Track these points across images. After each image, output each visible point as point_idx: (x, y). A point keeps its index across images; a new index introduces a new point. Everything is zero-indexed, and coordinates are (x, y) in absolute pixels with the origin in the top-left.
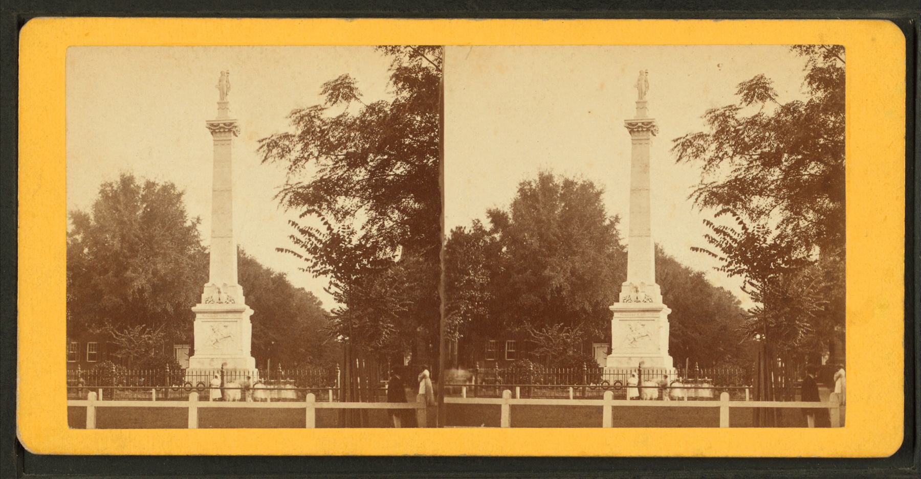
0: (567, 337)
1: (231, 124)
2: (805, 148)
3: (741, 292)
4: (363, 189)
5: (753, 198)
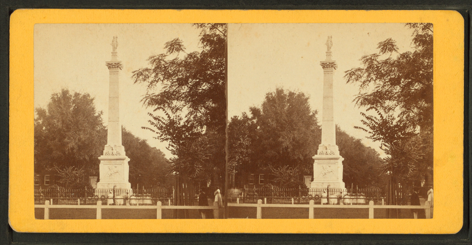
0: (77, 173)
1: (119, 63)
2: (413, 76)
3: (380, 149)
4: (186, 97)
5: (386, 101)
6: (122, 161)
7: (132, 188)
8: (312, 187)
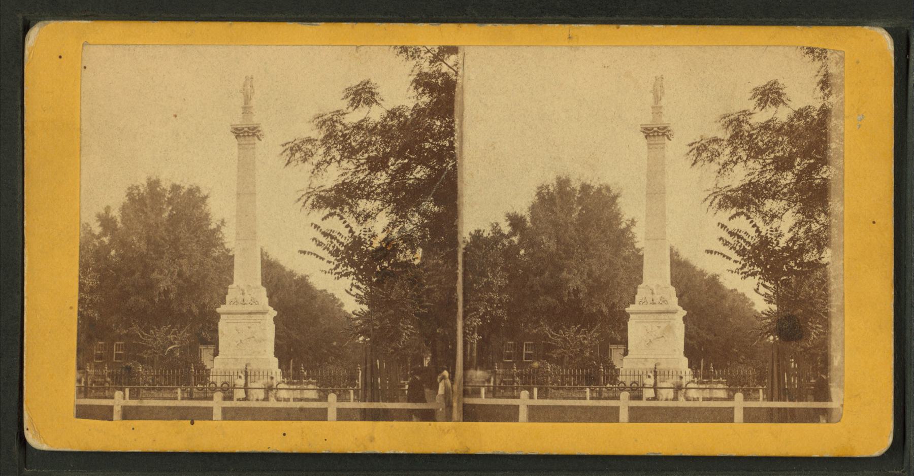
0: (585, 339)
1: (665, 128)
2: (818, 152)
3: (755, 296)
4: (384, 192)
5: (766, 202)
7: (280, 367)
8: (625, 367)
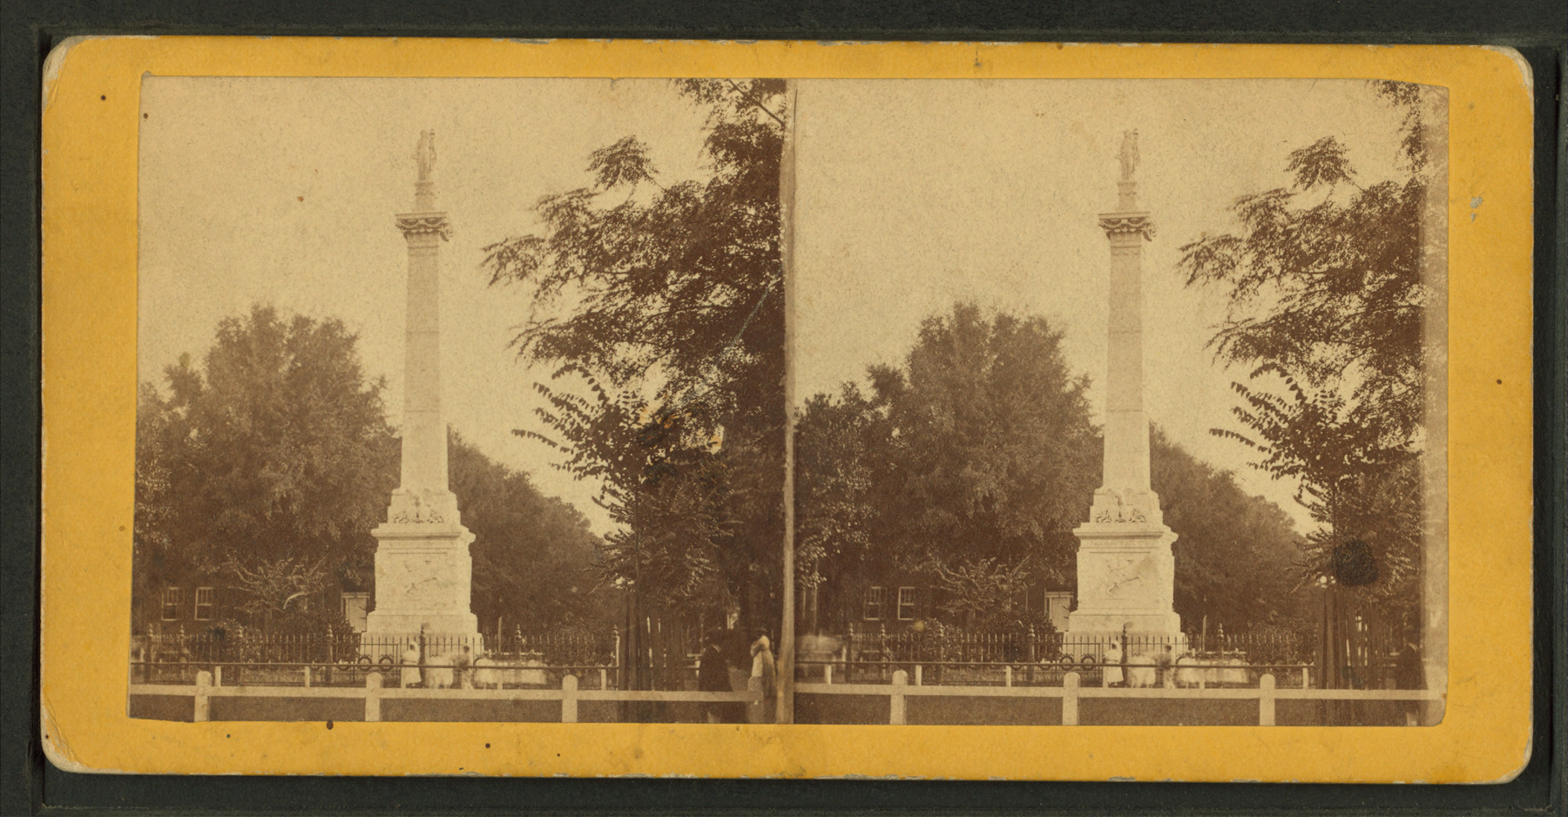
0: (1003, 581)
1: (1141, 219)
2: (1402, 262)
3: (1296, 508)
4: (660, 330)
5: (1314, 346)
6: (1150, 542)
7: (480, 631)
8: (1072, 629)
